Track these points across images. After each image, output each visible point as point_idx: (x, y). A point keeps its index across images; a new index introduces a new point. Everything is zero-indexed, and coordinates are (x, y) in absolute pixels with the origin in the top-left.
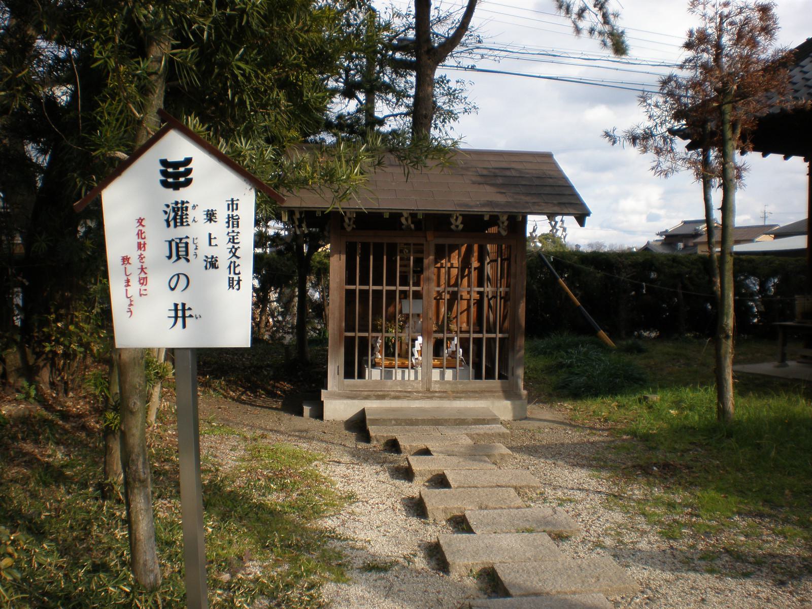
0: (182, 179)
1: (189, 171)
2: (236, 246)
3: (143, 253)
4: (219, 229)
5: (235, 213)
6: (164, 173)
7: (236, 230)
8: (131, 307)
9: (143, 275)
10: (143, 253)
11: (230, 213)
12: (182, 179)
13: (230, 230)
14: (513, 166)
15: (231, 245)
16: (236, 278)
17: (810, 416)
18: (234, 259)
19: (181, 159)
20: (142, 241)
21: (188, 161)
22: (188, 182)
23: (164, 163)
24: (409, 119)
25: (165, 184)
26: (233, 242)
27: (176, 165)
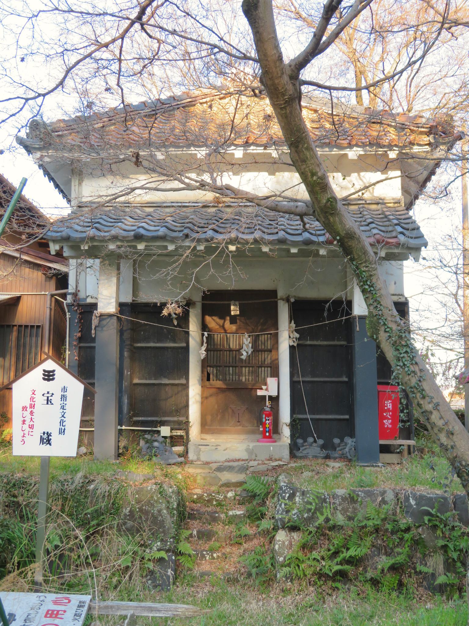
0: (51, 378)
1: (54, 375)
2: (65, 411)
3: (33, 409)
4: (55, 409)
5: (65, 394)
6: (44, 375)
7: (65, 403)
8: (24, 438)
9: (32, 423)
10: (33, 409)
11: (63, 393)
12: (51, 378)
13: (62, 402)
14: (48, 305)
15: (62, 410)
16: (63, 428)
17: (2, 261)
18: (63, 418)
19: (51, 369)
20: (33, 403)
21: (54, 371)
22: (53, 379)
23: (44, 371)
24: (459, 346)
25: (44, 379)
26: (63, 409)
27: (49, 372)
